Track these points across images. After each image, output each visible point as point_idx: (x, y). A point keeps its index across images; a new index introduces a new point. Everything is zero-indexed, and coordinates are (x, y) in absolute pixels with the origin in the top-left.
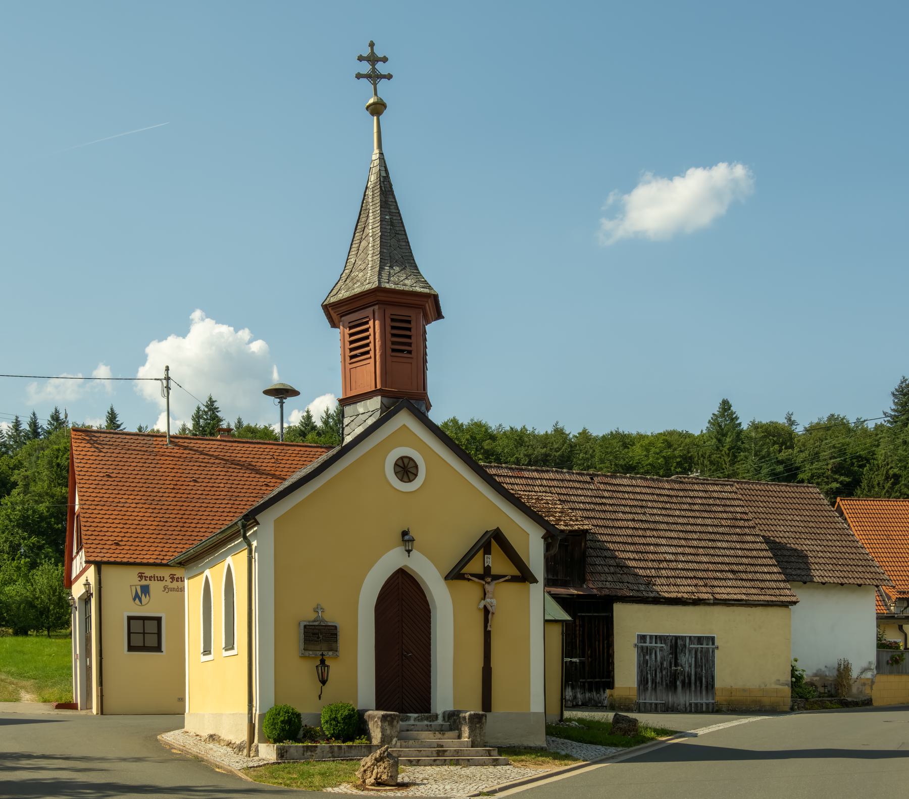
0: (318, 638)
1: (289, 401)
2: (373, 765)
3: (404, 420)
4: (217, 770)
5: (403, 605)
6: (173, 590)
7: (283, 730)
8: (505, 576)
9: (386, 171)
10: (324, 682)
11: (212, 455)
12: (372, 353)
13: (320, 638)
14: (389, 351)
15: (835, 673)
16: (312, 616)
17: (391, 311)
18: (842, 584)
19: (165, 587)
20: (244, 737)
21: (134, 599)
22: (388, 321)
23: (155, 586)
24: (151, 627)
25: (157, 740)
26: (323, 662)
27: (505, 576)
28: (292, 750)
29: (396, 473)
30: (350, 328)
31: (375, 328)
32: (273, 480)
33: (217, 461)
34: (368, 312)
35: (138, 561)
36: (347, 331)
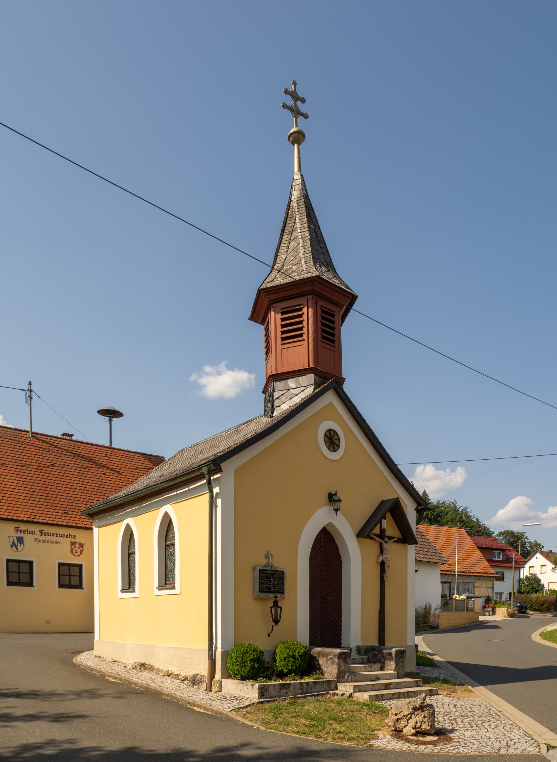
0: (270, 581)
1: (115, 420)
2: (411, 714)
3: (330, 398)
4: (196, 709)
5: (326, 554)
6: (42, 541)
7: (252, 668)
8: (394, 538)
9: (306, 190)
10: (276, 622)
11: (64, 449)
12: (305, 336)
13: (271, 582)
14: (320, 337)
15: (423, 611)
16: (264, 561)
17: (321, 303)
18: (429, 562)
19: (36, 539)
20: (203, 670)
21: (12, 547)
22: (319, 311)
23: (28, 538)
24: (25, 568)
25: (75, 665)
26: (276, 603)
27: (394, 538)
28: (271, 689)
29: (326, 442)
30: (283, 314)
31: (308, 315)
32: (108, 471)
33: (67, 453)
34: (303, 300)
35: (15, 518)
36: (279, 316)
